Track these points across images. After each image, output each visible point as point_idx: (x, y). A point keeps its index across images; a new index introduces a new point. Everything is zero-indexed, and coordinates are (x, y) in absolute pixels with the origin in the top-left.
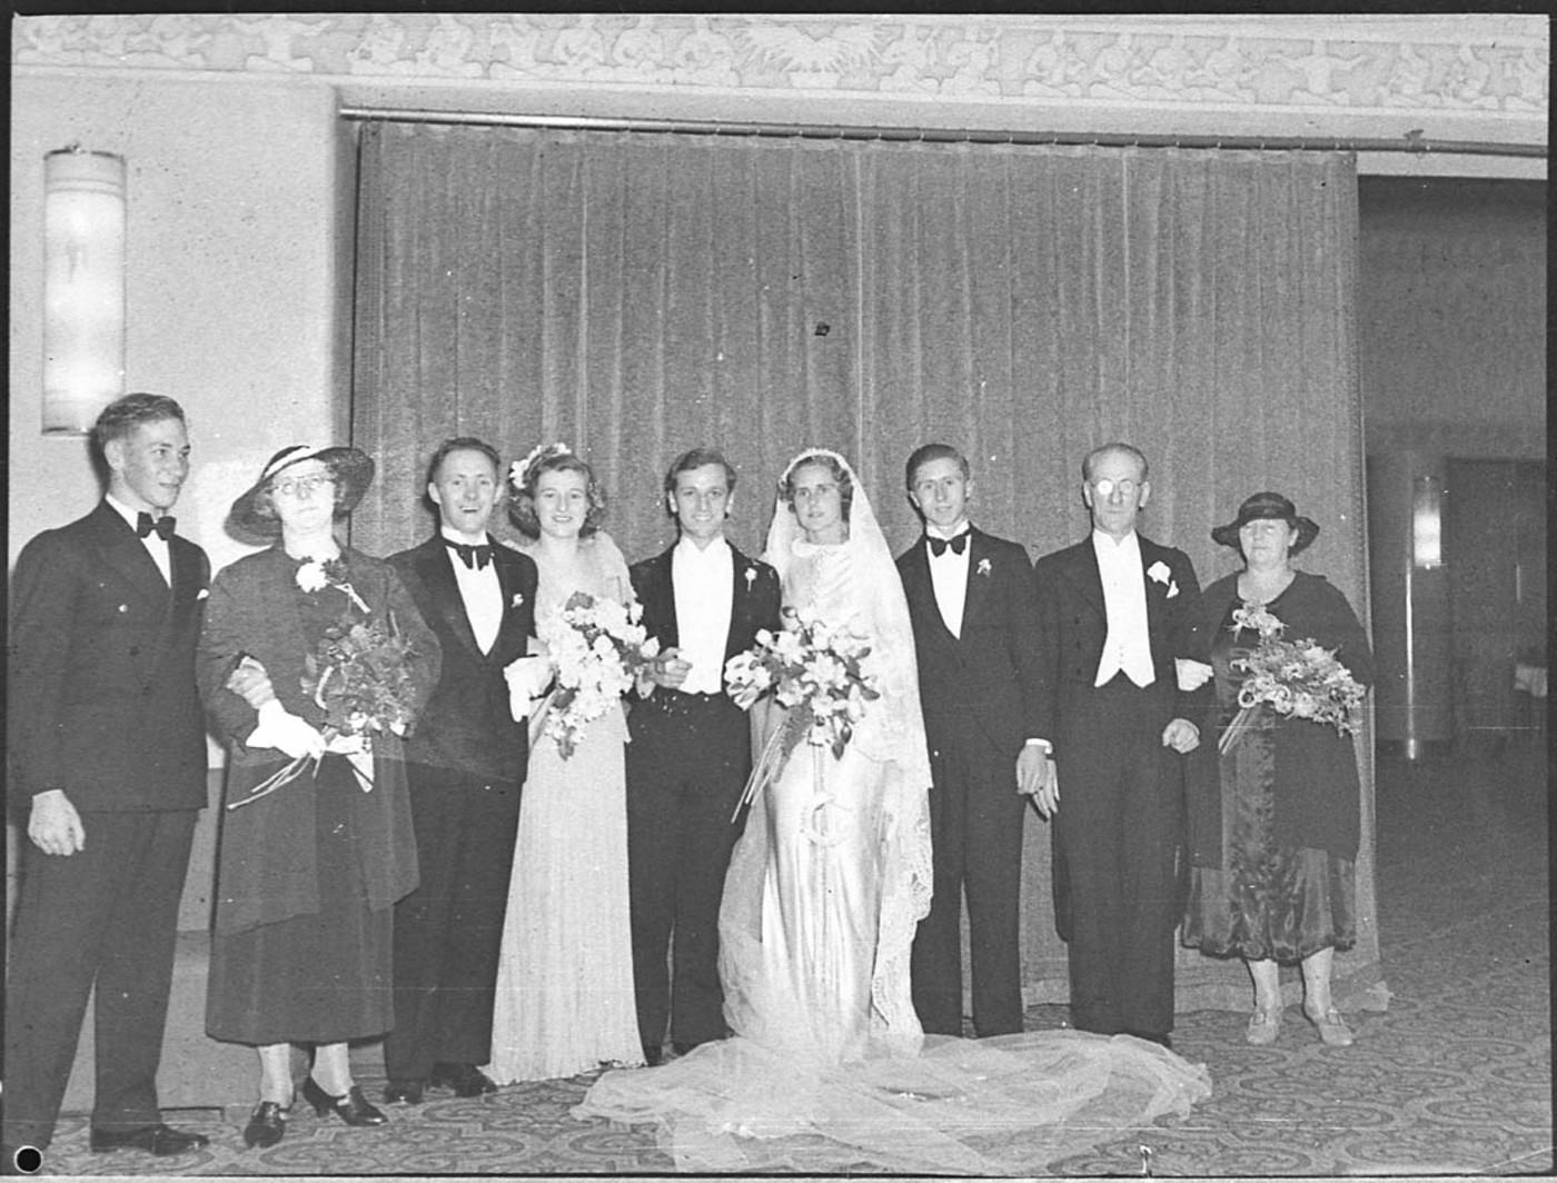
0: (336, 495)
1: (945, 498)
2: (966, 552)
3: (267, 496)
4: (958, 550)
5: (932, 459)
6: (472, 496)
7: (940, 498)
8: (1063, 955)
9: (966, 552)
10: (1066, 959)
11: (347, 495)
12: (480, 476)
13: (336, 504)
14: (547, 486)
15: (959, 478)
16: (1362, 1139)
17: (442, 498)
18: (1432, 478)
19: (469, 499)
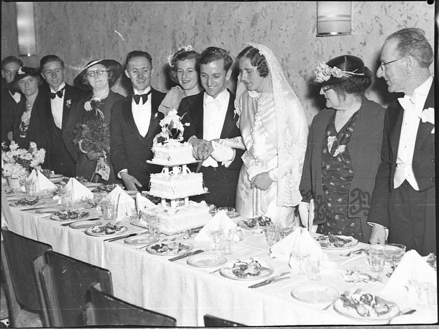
0: (109, 76)
1: (56, 77)
2: (63, 97)
3: (85, 78)
4: (60, 96)
5: (50, 61)
6: (141, 77)
7: (54, 77)
8: (433, 204)
9: (63, 97)
10: (435, 205)
11: (113, 76)
12: (143, 68)
13: (109, 80)
14: (203, 72)
15: (61, 69)
16: (100, 205)
17: (130, 76)
18: (26, 56)
19: (140, 78)
